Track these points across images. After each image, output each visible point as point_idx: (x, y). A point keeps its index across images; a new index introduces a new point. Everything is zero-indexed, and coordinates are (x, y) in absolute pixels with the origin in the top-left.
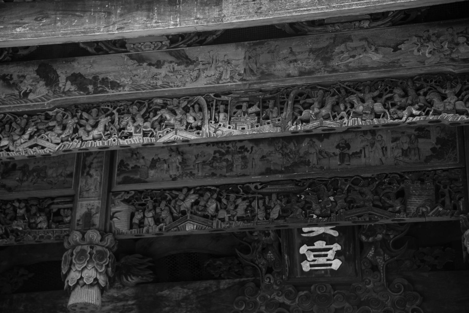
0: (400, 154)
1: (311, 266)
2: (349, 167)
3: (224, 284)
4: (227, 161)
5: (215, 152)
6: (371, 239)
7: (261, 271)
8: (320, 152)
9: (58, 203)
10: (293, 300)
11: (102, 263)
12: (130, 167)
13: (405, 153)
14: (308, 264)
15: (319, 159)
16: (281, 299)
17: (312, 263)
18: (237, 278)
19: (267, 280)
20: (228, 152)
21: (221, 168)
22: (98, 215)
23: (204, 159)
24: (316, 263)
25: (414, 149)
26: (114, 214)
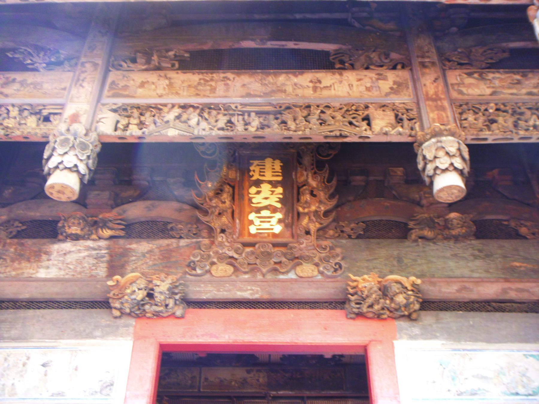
0: (364, 90)
1: (258, 229)
2: (321, 96)
3: (183, 242)
4: (211, 86)
5: (200, 79)
6: (306, 210)
8: (295, 84)
9: (48, 109)
10: (240, 254)
11: (83, 152)
12: (120, 86)
13: (368, 89)
15: (295, 89)
16: (232, 253)
18: (194, 238)
19: (221, 238)
20: (212, 80)
21: (205, 91)
22: (85, 116)
23: (190, 83)
25: (376, 87)
26: (100, 119)
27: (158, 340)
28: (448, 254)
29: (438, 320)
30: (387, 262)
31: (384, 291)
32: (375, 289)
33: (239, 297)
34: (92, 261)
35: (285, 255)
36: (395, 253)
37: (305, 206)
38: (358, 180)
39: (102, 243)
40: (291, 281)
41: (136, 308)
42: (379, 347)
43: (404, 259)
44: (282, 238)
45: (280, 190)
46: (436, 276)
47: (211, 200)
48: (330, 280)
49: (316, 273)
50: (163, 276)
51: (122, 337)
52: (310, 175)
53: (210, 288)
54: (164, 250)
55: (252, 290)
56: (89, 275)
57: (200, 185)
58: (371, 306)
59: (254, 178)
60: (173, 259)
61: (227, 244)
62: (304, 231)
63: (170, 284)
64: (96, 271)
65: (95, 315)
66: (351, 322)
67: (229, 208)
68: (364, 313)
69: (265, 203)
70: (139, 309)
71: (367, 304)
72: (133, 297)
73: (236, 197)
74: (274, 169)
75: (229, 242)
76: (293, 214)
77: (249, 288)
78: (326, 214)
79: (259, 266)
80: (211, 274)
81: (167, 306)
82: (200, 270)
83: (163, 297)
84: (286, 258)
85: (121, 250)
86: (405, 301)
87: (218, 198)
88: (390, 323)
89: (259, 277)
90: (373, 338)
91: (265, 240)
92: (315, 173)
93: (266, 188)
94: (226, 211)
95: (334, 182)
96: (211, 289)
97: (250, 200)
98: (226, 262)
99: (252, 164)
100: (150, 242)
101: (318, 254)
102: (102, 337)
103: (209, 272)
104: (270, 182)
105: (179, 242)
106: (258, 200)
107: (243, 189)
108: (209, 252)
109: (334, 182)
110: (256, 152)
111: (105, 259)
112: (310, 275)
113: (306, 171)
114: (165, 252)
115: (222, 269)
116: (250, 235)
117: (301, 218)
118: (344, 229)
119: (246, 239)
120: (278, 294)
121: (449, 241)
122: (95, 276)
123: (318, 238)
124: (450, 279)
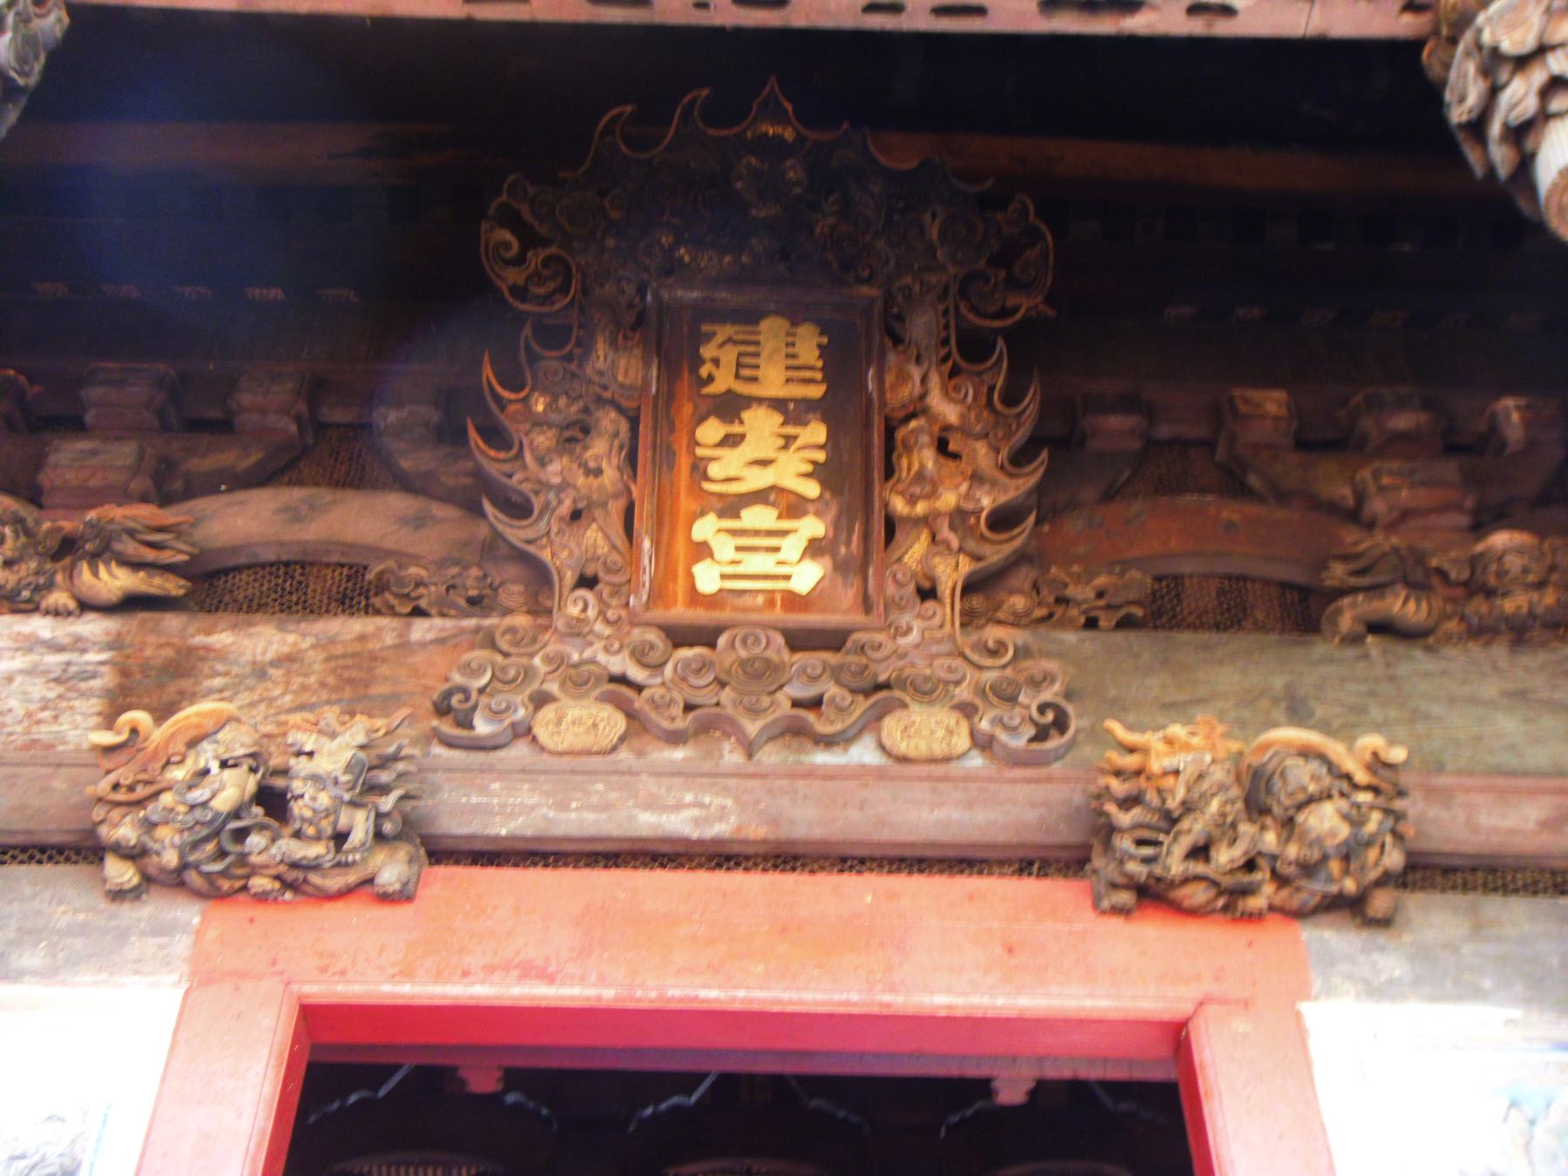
1: (724, 577)
3: (421, 630)
6: (921, 508)
7: (561, 579)
14: (716, 571)
16: (619, 663)
17: (730, 570)
24: (739, 569)
27: (295, 988)
28: (1491, 688)
29: (1478, 929)
30: (1247, 714)
31: (1258, 794)
32: (1218, 774)
33: (644, 832)
34: (39, 690)
35: (836, 674)
36: (1278, 682)
37: (917, 490)
38: (1116, 426)
39: (93, 627)
40: (861, 773)
41: (210, 847)
42: (1241, 1025)
43: (1312, 703)
44: (824, 610)
45: (816, 432)
46: (1450, 767)
47: (542, 462)
48: (1019, 773)
49: (962, 742)
50: (330, 715)
51: (137, 972)
52: (935, 380)
53: (526, 795)
54: (344, 656)
55: (701, 805)
56: (22, 740)
57: (499, 400)
58: (1201, 852)
59: (718, 387)
60: (379, 689)
61: (599, 627)
62: (911, 587)
63: (362, 747)
64: (55, 728)
65: (28, 891)
66: (1116, 923)
67: (616, 496)
68: (1172, 884)
69: (758, 479)
70: (222, 854)
71: (1185, 843)
72: (198, 795)
73: (644, 454)
74: (794, 356)
75: (608, 622)
76: (867, 523)
77: (689, 798)
78: (1002, 520)
79: (729, 710)
80: (534, 739)
81: (340, 838)
82: (490, 721)
83: (324, 800)
84: (839, 683)
85: (168, 653)
86: (1344, 831)
87: (571, 453)
88: (1276, 938)
89: (731, 756)
90: (1207, 987)
91: (755, 617)
92: (954, 373)
93: (761, 426)
94: (604, 505)
95: (1030, 404)
96: (535, 799)
97: (699, 470)
98: (597, 692)
99: (709, 337)
100: (291, 627)
101: (970, 673)
102: (49, 974)
103: (523, 732)
104: (778, 404)
105: (409, 626)
106: (730, 469)
107: (672, 429)
108: (532, 655)
109: (1030, 404)
110: (723, 295)
111: (96, 683)
112: (939, 749)
113: (918, 360)
114: (349, 662)
115: (581, 721)
116: (695, 597)
117: (899, 536)
118: (1070, 592)
119: (680, 613)
120: (805, 820)
121: (1487, 644)
122: (51, 746)
123: (969, 619)
124: (1509, 780)
